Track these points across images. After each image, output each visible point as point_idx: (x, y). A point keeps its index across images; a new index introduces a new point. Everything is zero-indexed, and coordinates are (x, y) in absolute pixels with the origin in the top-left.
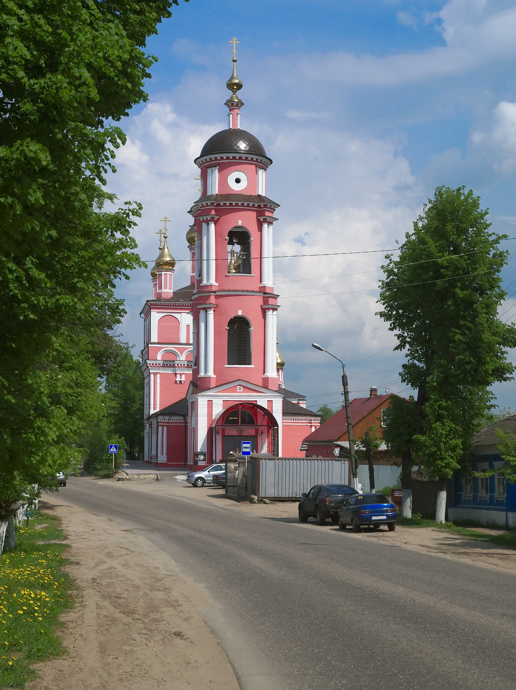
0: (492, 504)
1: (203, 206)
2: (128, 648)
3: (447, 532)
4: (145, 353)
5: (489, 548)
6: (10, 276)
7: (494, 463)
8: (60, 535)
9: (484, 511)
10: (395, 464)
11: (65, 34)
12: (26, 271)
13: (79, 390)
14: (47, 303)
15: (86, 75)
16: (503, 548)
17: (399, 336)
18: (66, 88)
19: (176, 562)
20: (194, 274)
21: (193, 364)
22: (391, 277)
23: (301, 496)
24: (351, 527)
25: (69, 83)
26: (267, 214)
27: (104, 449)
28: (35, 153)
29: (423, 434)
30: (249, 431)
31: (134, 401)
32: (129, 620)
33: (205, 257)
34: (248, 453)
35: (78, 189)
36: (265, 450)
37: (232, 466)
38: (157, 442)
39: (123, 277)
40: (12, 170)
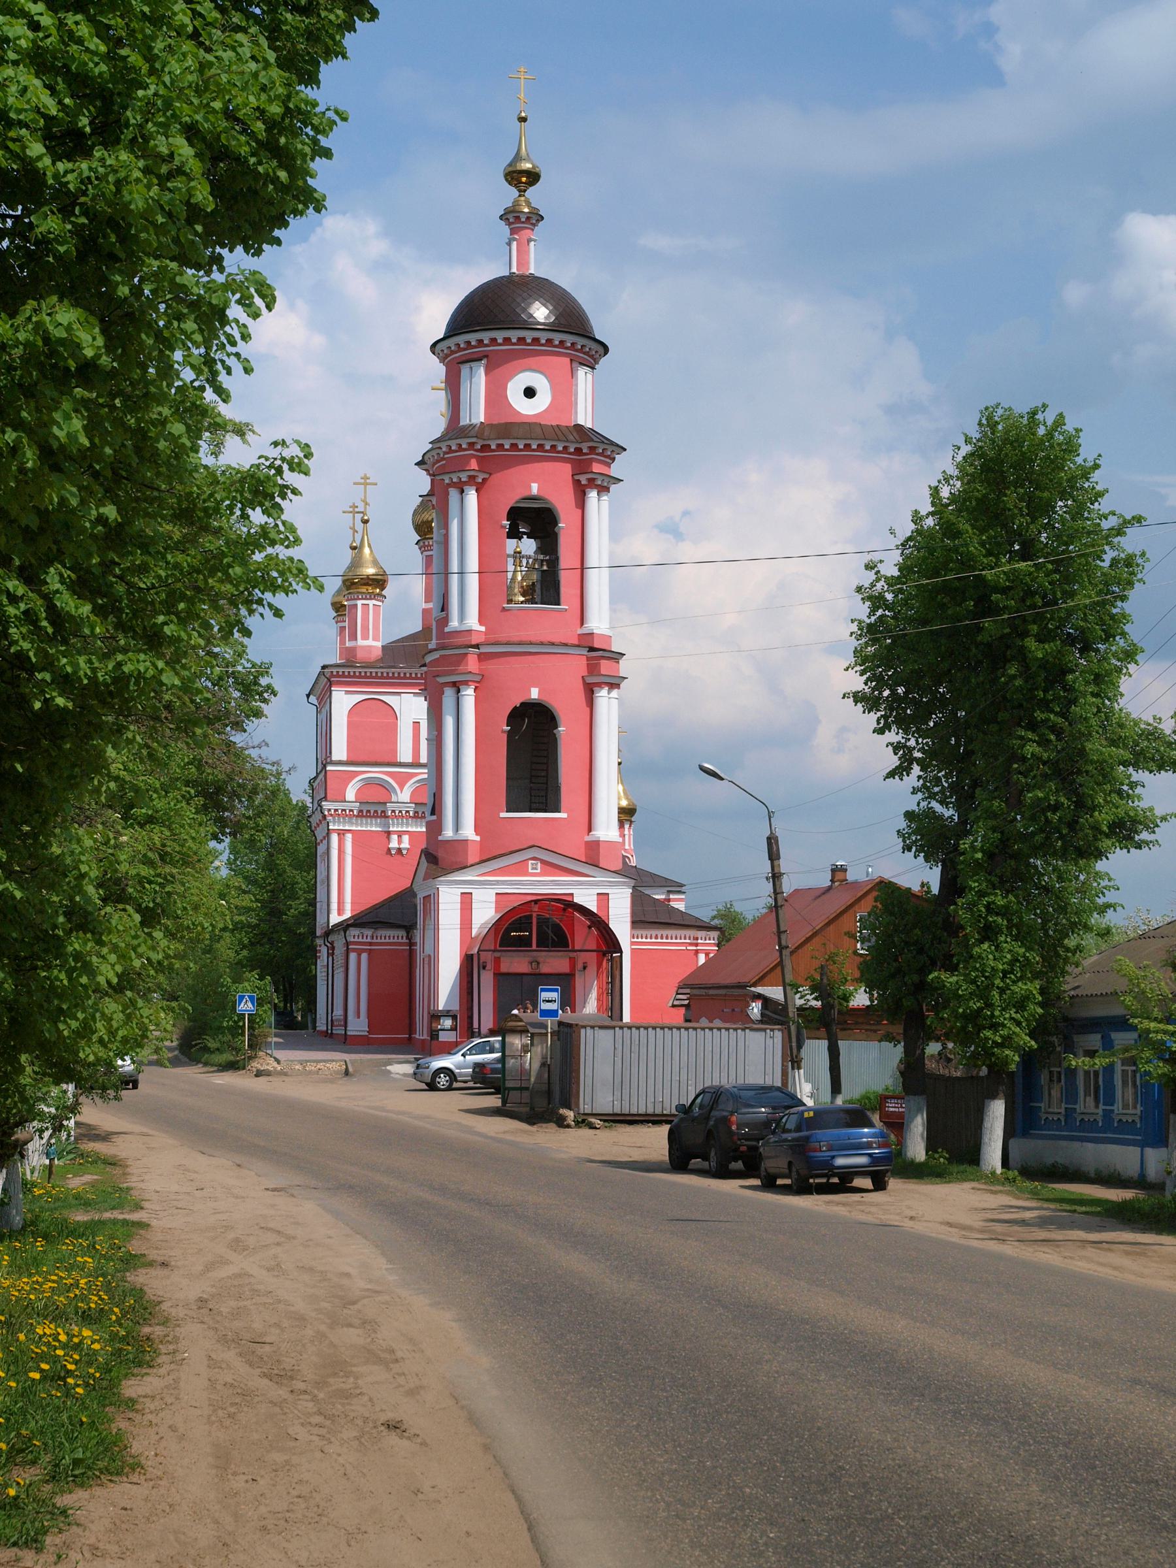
0: (1111, 1129)
1: (450, 451)
2: (279, 1457)
3: (1008, 1193)
4: (320, 784)
5: (1101, 1228)
6: (11, 611)
7: (1114, 1035)
8: (120, 1196)
9: (1090, 1145)
10: (889, 1038)
11: (135, 59)
12: (48, 598)
13: (168, 869)
14: (94, 670)
15: (185, 151)
16: (1134, 1230)
17: (896, 747)
18: (138, 180)
19: (390, 1261)
20: (430, 605)
21: (427, 814)
22: (880, 612)
23: (674, 1111)
24: (788, 1181)
25: (146, 171)
26: (597, 468)
27: (226, 1004)
28: (69, 328)
29: (952, 969)
30: (555, 962)
31: (293, 896)
32: (283, 1392)
33: (454, 566)
34: (553, 1013)
35: (166, 411)
36: (591, 1006)
37: (516, 1042)
38: (346, 986)
39: (268, 613)
40: (15, 369)
